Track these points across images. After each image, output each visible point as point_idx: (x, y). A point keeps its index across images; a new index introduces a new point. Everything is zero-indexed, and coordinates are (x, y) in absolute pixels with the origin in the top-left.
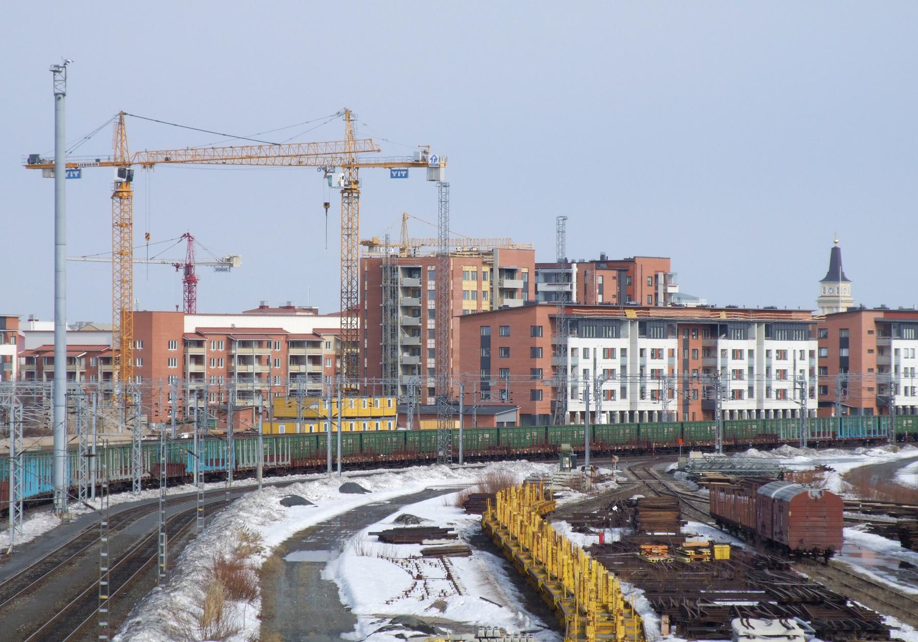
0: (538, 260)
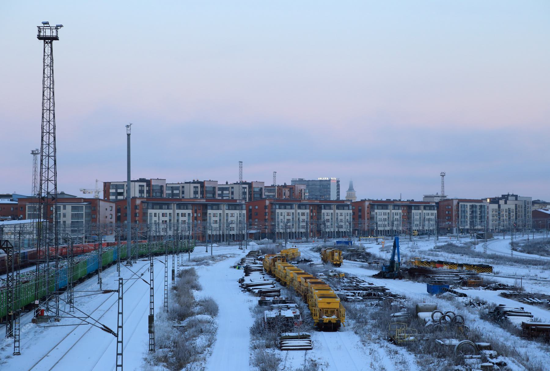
0: (533, 200)
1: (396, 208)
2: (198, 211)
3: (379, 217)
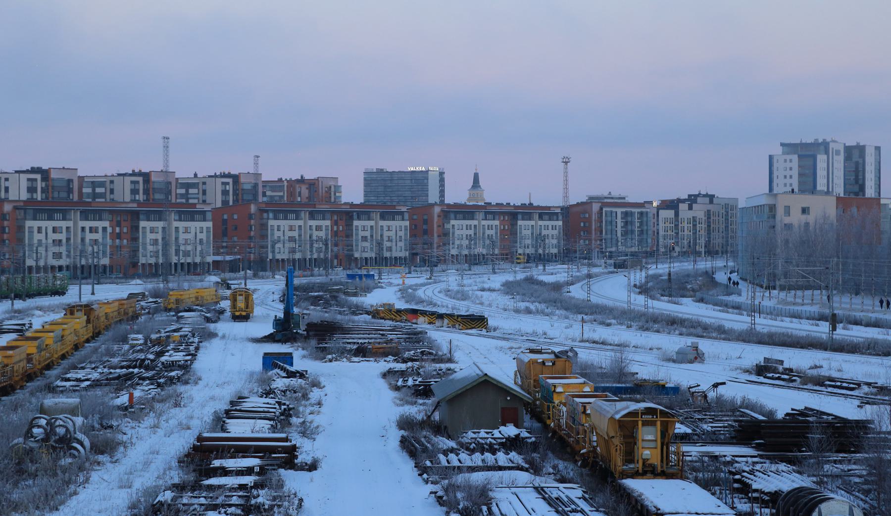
1: (489, 216)
2: (123, 223)
3: (457, 232)
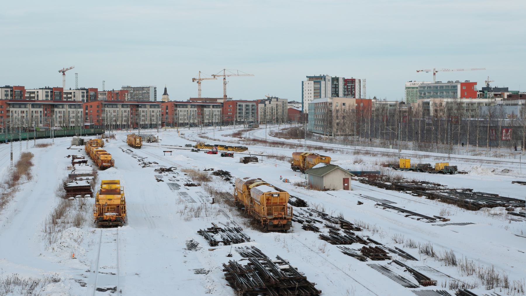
2: (48, 109)
3: (180, 113)
